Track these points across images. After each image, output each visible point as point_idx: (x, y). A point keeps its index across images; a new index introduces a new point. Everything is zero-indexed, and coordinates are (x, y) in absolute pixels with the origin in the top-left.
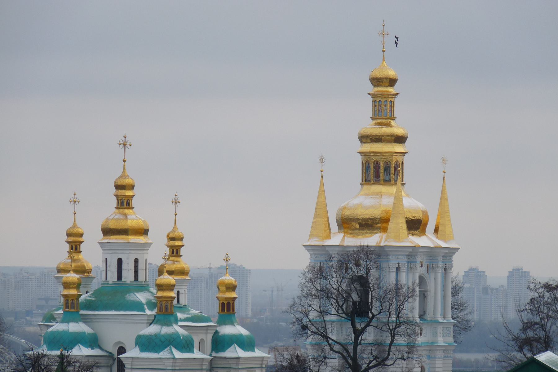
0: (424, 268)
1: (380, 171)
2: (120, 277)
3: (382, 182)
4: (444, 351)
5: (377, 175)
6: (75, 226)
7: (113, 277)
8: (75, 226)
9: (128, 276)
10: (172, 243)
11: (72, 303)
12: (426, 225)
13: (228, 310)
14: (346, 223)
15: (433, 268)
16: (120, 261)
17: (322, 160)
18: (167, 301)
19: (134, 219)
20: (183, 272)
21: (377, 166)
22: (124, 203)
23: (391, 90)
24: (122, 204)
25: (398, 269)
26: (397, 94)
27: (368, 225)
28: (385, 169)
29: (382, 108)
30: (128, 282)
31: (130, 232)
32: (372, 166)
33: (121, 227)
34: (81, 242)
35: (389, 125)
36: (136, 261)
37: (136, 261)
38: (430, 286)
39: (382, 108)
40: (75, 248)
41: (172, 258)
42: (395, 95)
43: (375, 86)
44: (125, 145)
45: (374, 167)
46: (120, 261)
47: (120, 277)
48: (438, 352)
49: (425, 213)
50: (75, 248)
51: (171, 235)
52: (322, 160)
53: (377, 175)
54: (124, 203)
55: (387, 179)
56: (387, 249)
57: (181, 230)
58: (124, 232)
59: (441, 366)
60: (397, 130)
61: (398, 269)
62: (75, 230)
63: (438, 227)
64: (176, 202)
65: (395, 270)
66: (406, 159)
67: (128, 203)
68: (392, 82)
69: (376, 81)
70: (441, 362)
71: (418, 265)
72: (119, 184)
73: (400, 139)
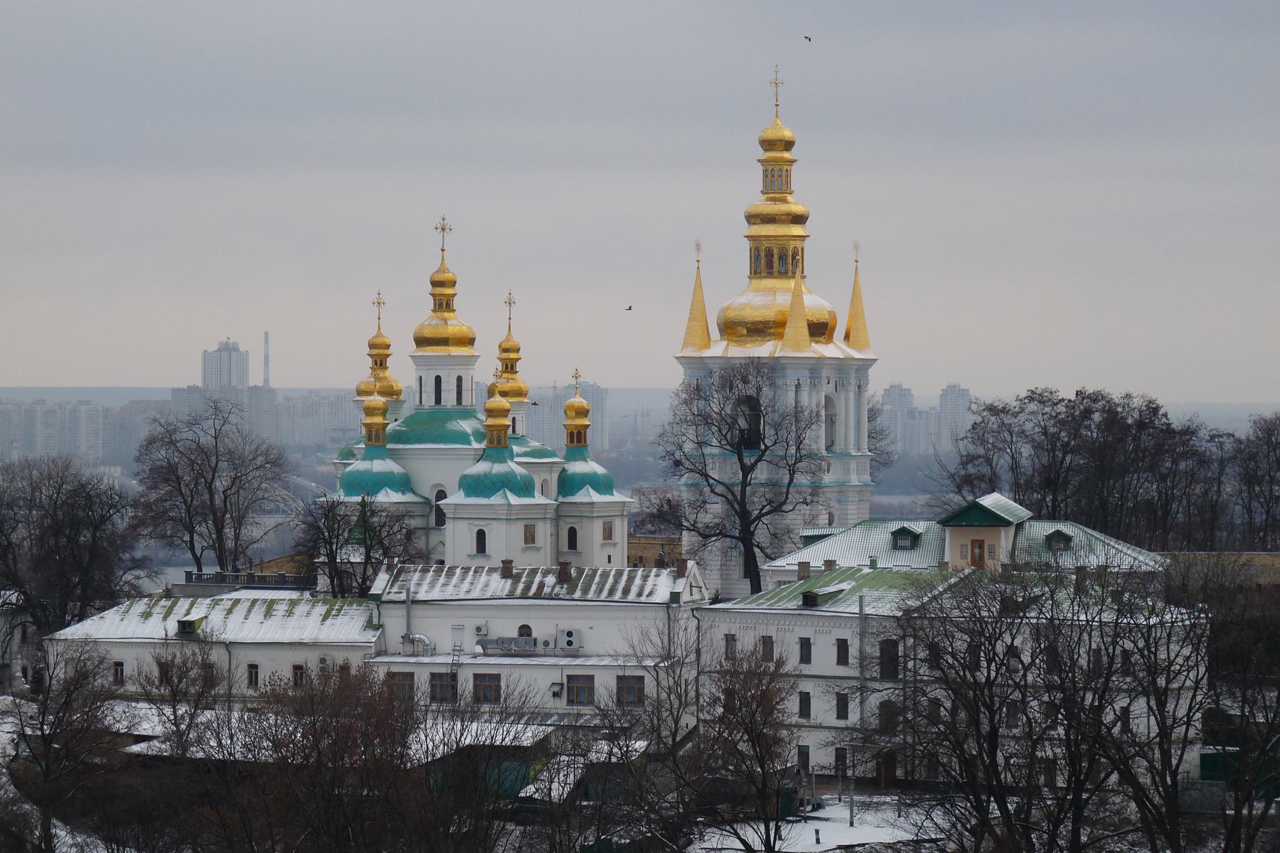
0: (832, 385)
1: (773, 260)
2: (438, 400)
5: (770, 265)
6: (379, 334)
8: (379, 334)
9: (449, 398)
10: (505, 355)
12: (833, 329)
14: (730, 328)
16: (438, 379)
17: (698, 247)
19: (456, 324)
20: (520, 393)
21: (769, 254)
22: (443, 304)
23: (786, 155)
24: (441, 305)
25: (798, 386)
27: (759, 330)
28: (780, 258)
29: (776, 178)
30: (449, 407)
32: (763, 254)
34: (388, 356)
36: (459, 379)
37: (459, 379)
40: (380, 362)
41: (505, 375)
42: (792, 162)
43: (766, 150)
46: (438, 379)
49: (833, 315)
51: (505, 346)
52: (698, 247)
53: (770, 265)
54: (443, 304)
56: (783, 361)
58: (443, 341)
61: (798, 386)
62: (379, 341)
64: (510, 303)
68: (788, 145)
69: (768, 144)
73: (799, 219)
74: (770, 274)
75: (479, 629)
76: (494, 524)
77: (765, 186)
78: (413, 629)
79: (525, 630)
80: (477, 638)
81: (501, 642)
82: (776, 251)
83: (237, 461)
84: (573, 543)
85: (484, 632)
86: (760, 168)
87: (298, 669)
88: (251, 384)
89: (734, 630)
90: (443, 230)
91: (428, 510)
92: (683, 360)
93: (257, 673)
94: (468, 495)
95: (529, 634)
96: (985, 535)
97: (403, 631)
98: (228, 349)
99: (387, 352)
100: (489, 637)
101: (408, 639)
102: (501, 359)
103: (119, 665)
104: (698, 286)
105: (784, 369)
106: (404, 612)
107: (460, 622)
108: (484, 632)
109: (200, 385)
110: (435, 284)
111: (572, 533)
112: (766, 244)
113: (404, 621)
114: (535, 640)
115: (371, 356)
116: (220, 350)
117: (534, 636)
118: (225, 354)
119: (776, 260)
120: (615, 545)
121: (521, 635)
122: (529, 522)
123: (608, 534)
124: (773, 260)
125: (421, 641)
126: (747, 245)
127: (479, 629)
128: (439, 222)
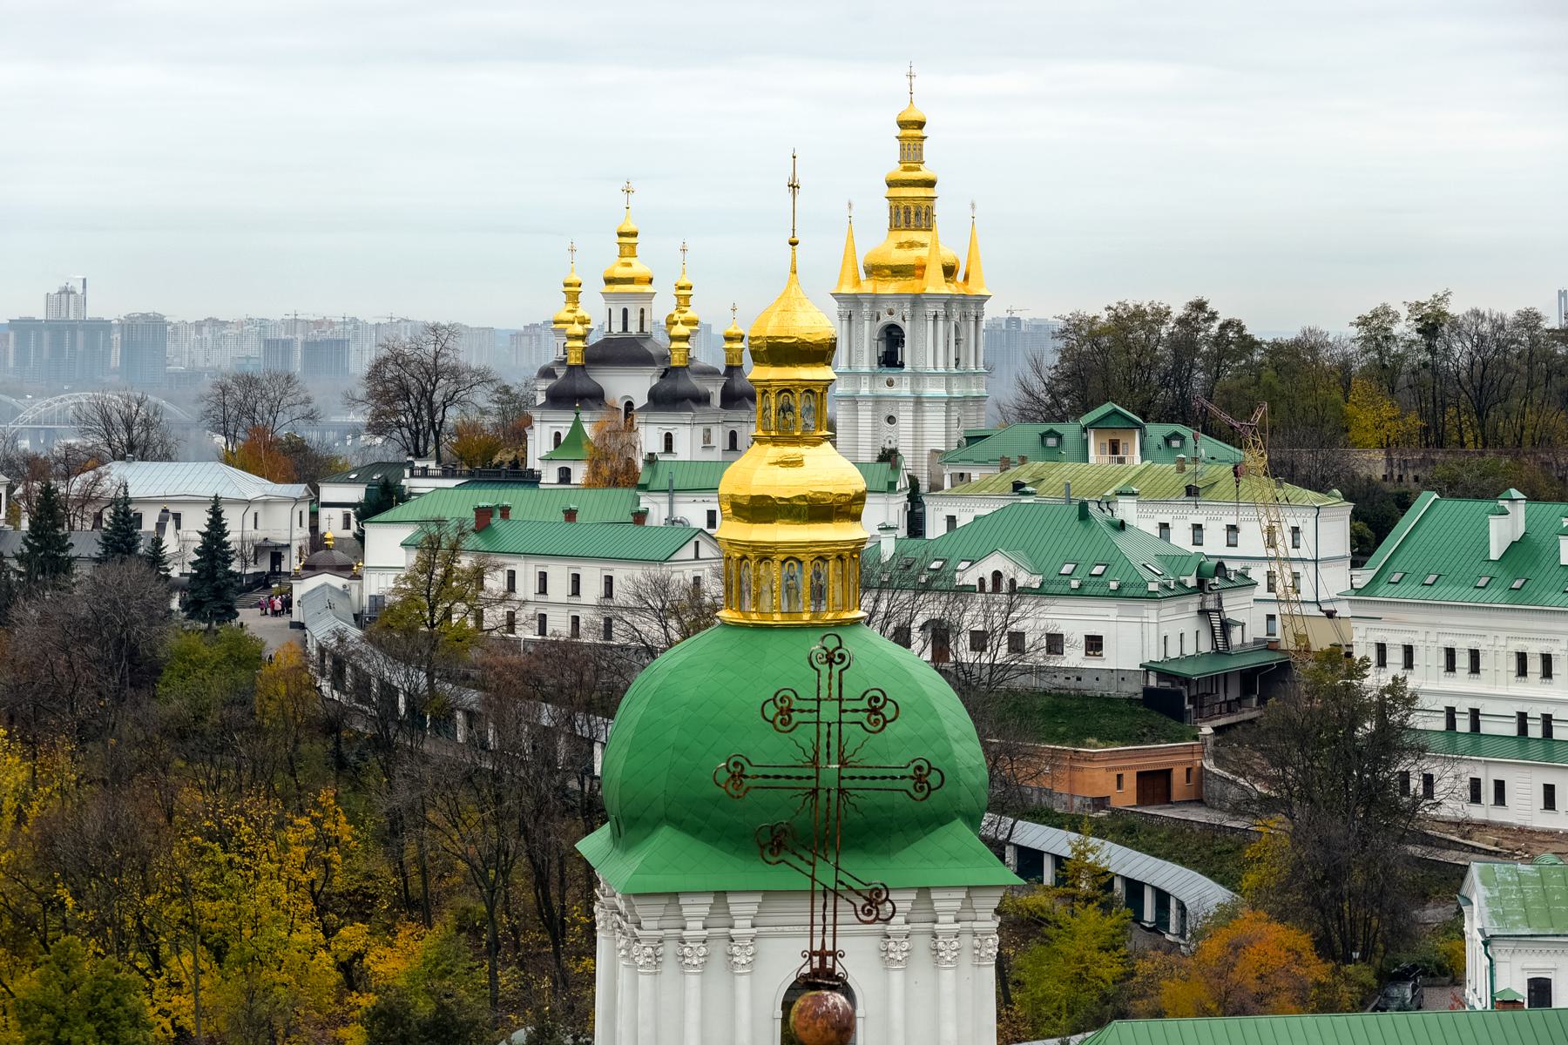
1: (912, 214)
5: (908, 222)
7: (617, 328)
14: (874, 270)
16: (625, 311)
17: (973, 206)
19: (638, 268)
20: (695, 323)
21: (907, 211)
25: (936, 317)
27: (899, 271)
40: (573, 298)
46: (625, 311)
50: (573, 298)
52: (973, 206)
53: (908, 222)
58: (630, 281)
61: (936, 317)
69: (903, 125)
70: (655, 924)
73: (930, 184)
74: (908, 227)
76: (681, 428)
77: (902, 156)
83: (454, 373)
86: (897, 142)
92: (838, 296)
94: (1217, 764)
99: (648, 289)
104: (851, 237)
110: (903, 125)
112: (904, 203)
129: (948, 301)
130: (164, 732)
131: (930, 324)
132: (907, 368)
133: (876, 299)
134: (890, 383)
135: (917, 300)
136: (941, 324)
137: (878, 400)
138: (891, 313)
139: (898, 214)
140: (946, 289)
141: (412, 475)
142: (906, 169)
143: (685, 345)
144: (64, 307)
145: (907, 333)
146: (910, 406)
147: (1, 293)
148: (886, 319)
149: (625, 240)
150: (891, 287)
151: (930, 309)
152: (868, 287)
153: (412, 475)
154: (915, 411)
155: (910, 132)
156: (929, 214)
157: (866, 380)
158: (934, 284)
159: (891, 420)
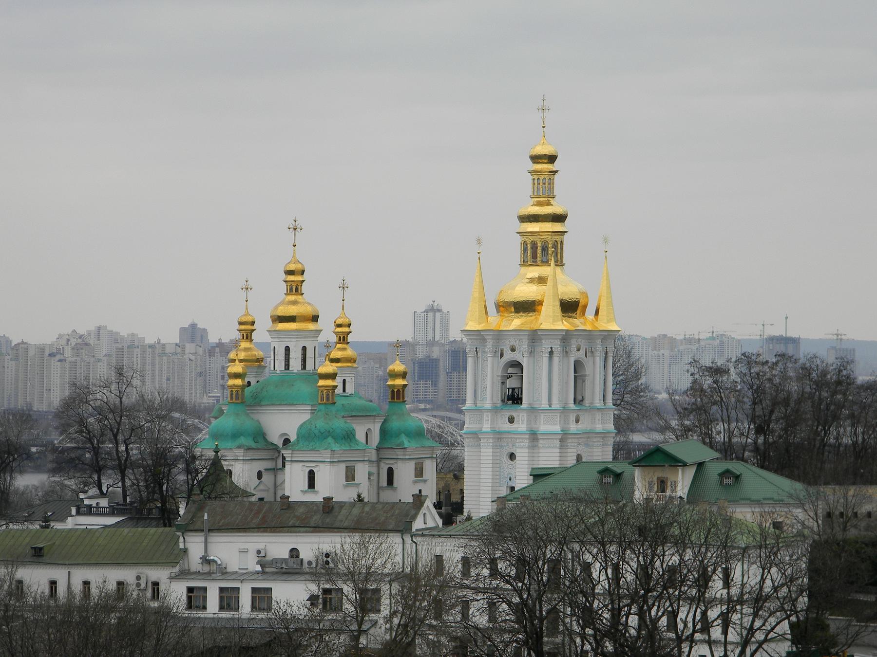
0: (582, 352)
1: (541, 252)
2: (287, 366)
3: (539, 263)
4: (603, 438)
5: (534, 256)
8: (247, 314)
9: (295, 364)
11: (237, 394)
12: (585, 307)
13: (398, 398)
15: (592, 352)
16: (287, 349)
17: (479, 241)
18: (328, 390)
21: (534, 246)
22: (295, 289)
24: (291, 290)
26: (557, 172)
29: (544, 186)
30: (295, 371)
31: (297, 319)
32: (529, 247)
33: (288, 315)
34: (253, 330)
35: (549, 204)
38: (588, 370)
39: (544, 186)
41: (339, 346)
42: (554, 172)
43: (534, 163)
44: (295, 229)
45: (532, 248)
46: (287, 349)
47: (287, 366)
48: (570, 441)
49: (585, 294)
52: (479, 241)
53: (534, 256)
54: (295, 289)
55: (545, 260)
57: (351, 315)
58: (291, 319)
59: (600, 454)
60: (555, 208)
63: (279, 317)
64: (343, 288)
65: (547, 355)
66: (566, 238)
67: (297, 288)
68: (552, 159)
69: (536, 159)
71: (574, 348)
72: (288, 269)
73: (559, 218)
75: (259, 552)
76: (321, 465)
78: (210, 552)
79: (294, 553)
80: (258, 559)
81: (275, 561)
82: (539, 244)
84: (390, 481)
85: (262, 554)
86: (530, 177)
87: (120, 584)
88: (451, 339)
89: (261, 546)
90: (295, 229)
91: (276, 455)
93: (158, 589)
95: (298, 556)
96: (666, 473)
97: (202, 553)
98: (433, 310)
100: (267, 558)
101: (206, 560)
102: (336, 333)
103: (156, 584)
105: (541, 339)
106: (203, 539)
107: (243, 546)
108: (262, 554)
109: (411, 340)
111: (390, 472)
112: (532, 238)
113: (203, 545)
114: (302, 560)
115: (239, 331)
116: (426, 311)
117: (301, 557)
118: (430, 314)
119: (539, 251)
120: (425, 481)
121: (291, 556)
122: (349, 464)
123: (419, 472)
124: (541, 252)
125: (214, 561)
126: (519, 239)
127: (259, 552)
128: (291, 223)
129: (566, 337)
130: (866, 545)
131: (546, 360)
132: (525, 405)
133: (499, 335)
134: (511, 420)
135: (535, 337)
136: (556, 360)
137: (499, 436)
138: (513, 350)
139: (525, 249)
140: (563, 325)
141: (79, 513)
142: (539, 204)
143: (329, 382)
144: (430, 325)
145: (525, 365)
146: (526, 443)
147: (38, 325)
148: (509, 356)
149: (291, 278)
150: (517, 322)
151: (546, 345)
152: (495, 321)
153: (79, 513)
154: (561, 447)
155: (539, 167)
156: (558, 248)
157: (487, 416)
158: (550, 319)
159: (512, 456)
